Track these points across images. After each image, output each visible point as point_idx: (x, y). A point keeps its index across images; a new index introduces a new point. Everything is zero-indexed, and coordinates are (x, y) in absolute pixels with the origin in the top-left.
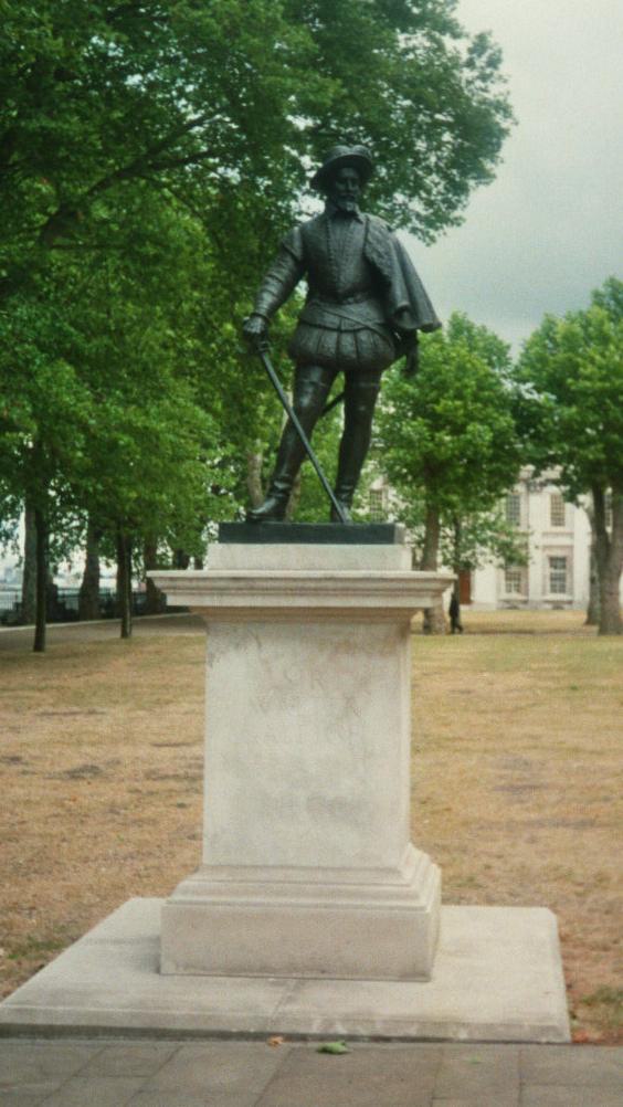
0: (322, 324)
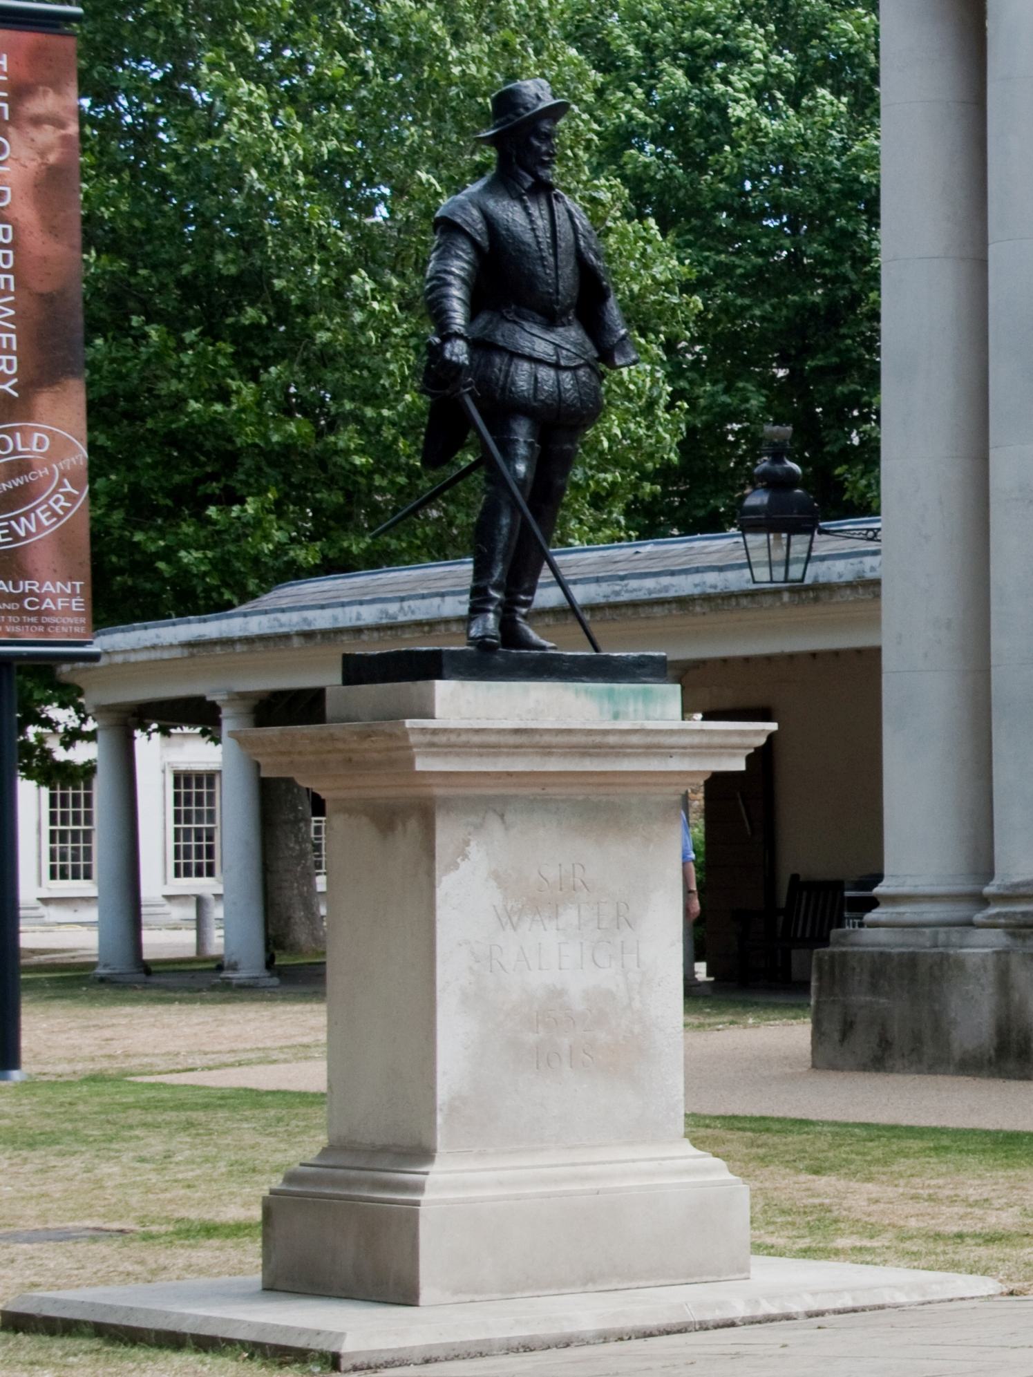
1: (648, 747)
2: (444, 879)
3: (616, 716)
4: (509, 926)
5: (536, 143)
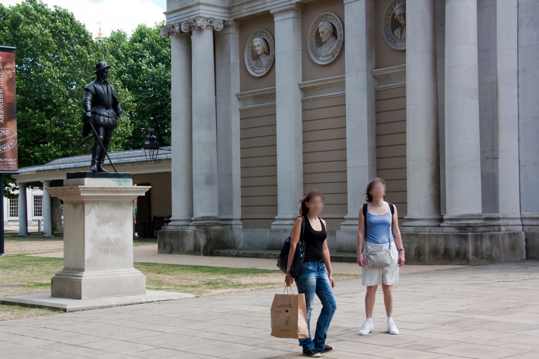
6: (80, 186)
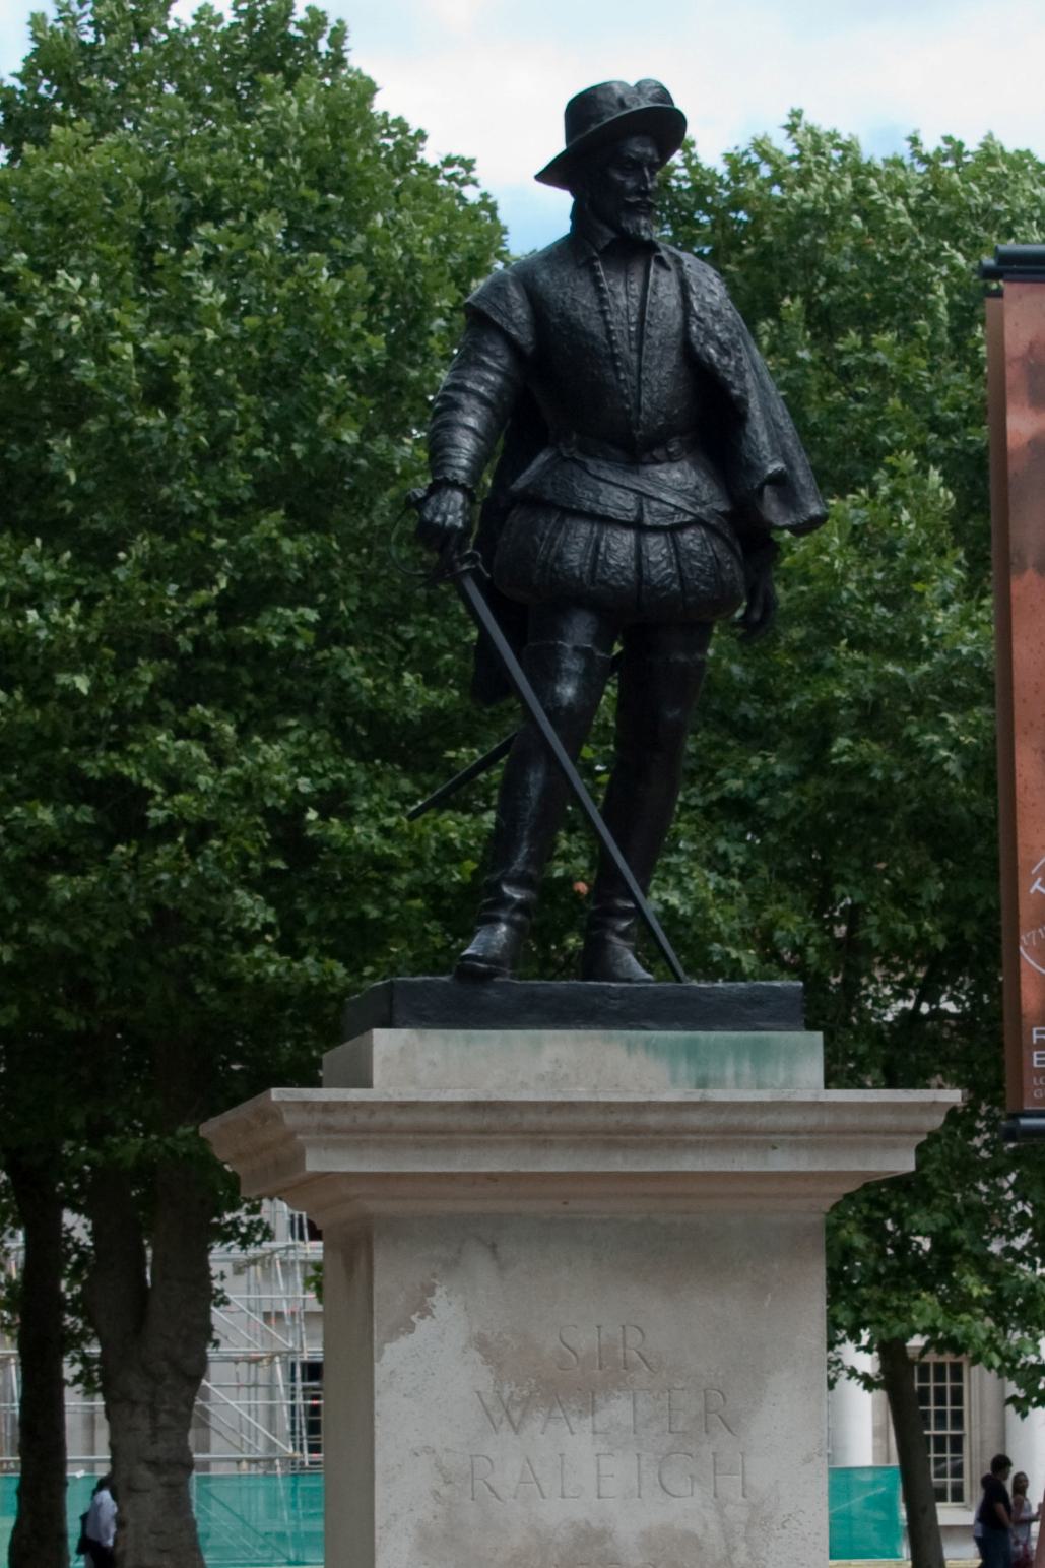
0: (599, 510)
1: (728, 1131)
2: (387, 1347)
3: (702, 1083)
4: (505, 1424)
5: (618, 177)
6: (276, 1094)
